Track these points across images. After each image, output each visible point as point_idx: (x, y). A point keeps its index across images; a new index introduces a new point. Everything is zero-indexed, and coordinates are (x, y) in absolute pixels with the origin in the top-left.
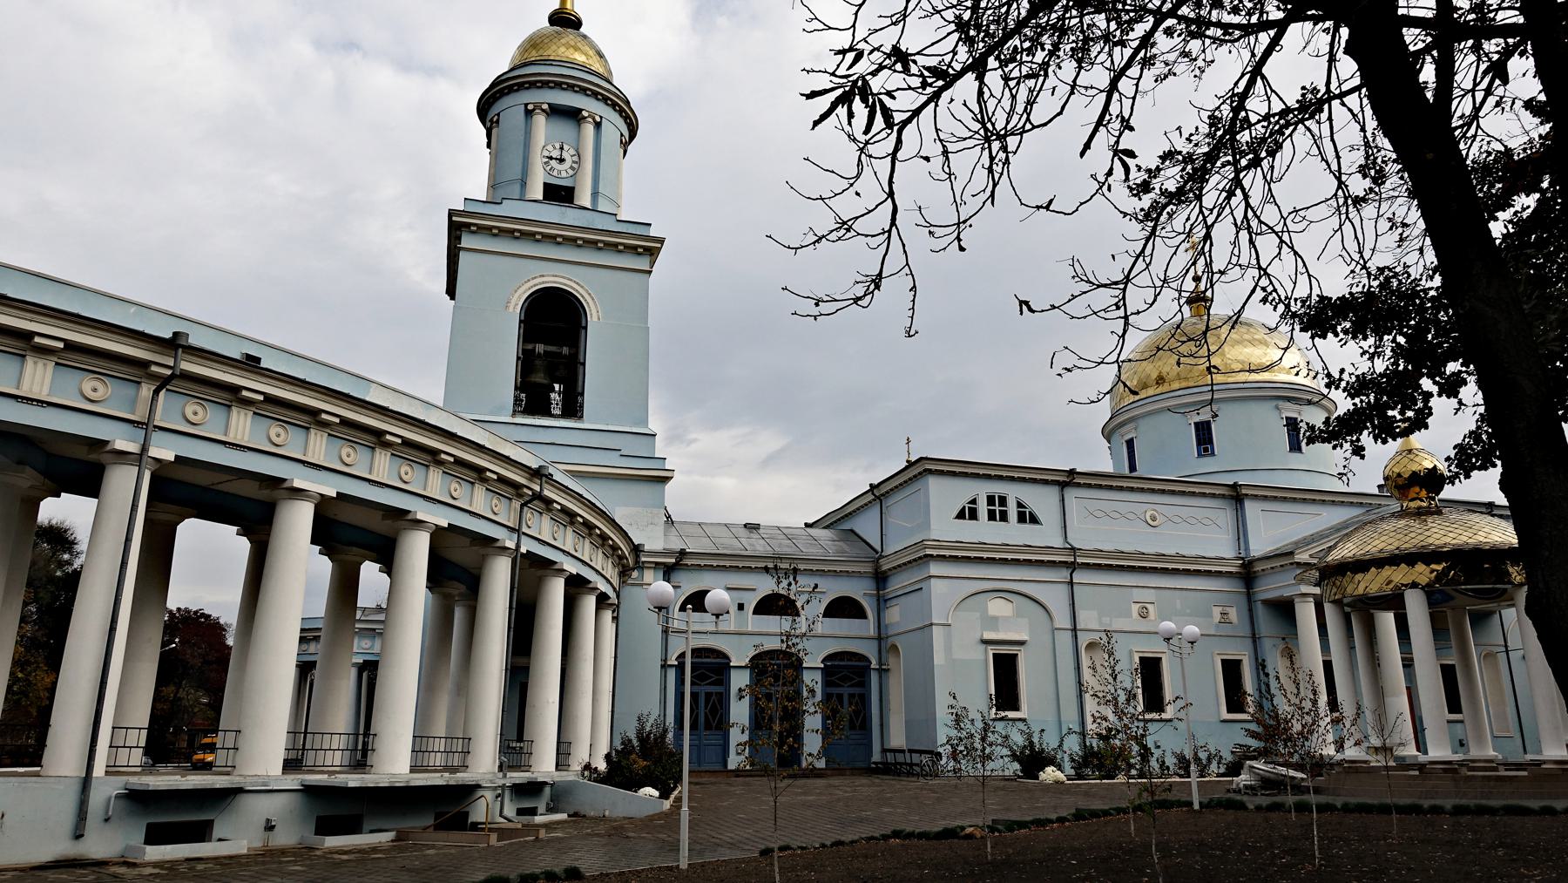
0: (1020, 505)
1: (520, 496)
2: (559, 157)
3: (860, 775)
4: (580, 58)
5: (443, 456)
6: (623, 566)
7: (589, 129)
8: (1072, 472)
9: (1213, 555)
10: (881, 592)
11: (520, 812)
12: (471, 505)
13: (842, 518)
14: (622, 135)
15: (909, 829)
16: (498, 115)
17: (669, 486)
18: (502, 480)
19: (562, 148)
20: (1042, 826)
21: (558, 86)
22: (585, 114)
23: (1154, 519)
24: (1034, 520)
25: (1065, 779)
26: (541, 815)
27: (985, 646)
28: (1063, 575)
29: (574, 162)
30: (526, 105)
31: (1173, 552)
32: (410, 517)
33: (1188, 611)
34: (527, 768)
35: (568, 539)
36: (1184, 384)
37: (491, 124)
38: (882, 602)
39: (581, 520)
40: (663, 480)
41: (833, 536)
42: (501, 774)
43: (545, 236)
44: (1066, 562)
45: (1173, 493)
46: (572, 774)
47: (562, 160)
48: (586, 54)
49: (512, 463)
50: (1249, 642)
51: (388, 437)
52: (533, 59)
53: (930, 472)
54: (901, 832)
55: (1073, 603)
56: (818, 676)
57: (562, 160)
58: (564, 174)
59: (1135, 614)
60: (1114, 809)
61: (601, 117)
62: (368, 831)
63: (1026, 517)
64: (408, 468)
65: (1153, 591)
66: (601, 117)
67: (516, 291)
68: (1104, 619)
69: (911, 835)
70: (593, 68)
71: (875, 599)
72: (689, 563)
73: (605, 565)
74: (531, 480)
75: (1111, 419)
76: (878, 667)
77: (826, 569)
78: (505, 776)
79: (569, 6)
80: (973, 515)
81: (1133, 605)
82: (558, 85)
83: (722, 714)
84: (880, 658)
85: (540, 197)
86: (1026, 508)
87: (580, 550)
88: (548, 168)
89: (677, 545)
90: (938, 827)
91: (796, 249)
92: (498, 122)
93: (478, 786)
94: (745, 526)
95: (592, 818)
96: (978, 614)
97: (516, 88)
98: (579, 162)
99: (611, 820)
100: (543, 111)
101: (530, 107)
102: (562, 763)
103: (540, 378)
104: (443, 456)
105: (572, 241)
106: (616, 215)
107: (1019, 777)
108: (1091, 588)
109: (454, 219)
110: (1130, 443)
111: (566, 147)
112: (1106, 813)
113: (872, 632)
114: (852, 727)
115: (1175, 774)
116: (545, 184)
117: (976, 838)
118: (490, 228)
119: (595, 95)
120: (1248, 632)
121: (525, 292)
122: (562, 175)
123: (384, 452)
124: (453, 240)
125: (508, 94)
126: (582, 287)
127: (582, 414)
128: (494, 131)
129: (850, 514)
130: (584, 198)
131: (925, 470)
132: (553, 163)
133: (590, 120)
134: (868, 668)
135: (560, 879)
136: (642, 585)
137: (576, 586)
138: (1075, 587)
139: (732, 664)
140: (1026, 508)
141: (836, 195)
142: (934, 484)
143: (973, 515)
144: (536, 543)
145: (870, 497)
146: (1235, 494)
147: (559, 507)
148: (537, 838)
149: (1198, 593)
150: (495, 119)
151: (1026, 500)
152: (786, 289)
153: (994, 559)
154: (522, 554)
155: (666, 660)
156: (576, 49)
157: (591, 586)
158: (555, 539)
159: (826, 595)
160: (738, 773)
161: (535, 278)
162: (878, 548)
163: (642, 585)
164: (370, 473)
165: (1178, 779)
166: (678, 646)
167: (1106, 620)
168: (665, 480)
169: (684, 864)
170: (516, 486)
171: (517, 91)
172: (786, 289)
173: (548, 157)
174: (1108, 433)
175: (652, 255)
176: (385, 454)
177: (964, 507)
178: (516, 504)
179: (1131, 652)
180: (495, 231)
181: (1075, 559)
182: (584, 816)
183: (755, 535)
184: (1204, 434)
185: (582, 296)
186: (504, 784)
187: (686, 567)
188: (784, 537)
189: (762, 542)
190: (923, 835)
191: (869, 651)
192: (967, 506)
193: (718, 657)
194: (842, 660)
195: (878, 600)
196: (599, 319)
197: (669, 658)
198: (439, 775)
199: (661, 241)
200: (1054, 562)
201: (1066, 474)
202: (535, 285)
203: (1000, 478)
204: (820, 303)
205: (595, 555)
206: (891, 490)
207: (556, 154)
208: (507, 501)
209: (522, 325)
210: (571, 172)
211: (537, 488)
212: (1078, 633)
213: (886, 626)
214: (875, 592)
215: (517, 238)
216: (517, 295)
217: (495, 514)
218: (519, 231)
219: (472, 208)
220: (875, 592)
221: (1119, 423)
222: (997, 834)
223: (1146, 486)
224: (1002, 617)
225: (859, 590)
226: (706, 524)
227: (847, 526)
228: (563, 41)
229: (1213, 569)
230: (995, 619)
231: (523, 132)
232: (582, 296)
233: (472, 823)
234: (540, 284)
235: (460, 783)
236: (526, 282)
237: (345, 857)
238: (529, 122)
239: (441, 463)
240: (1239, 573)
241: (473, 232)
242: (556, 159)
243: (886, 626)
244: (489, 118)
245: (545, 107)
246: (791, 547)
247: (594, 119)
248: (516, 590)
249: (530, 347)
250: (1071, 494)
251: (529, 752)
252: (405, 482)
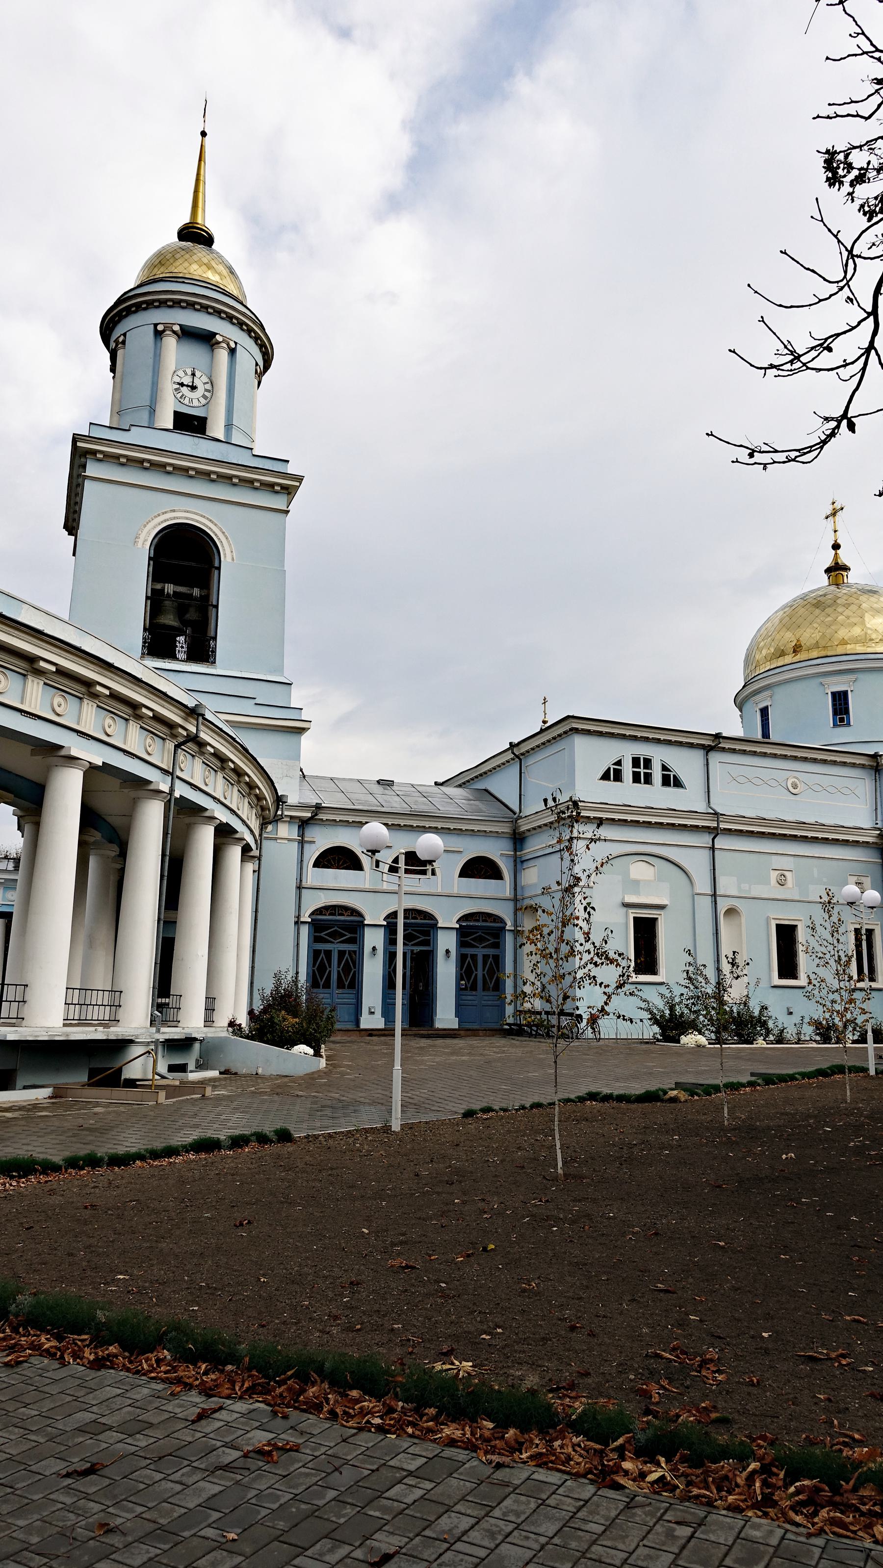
0: (664, 768)
1: (174, 736)
2: (190, 384)
3: (485, 1035)
4: (213, 277)
5: (99, 688)
6: (264, 818)
7: (222, 354)
8: (718, 736)
9: (851, 825)
10: (518, 853)
11: (172, 1068)
12: (125, 744)
13: (476, 777)
14: (257, 364)
15: (606, 1091)
16: (125, 335)
17: (305, 738)
18: (158, 718)
19: (193, 375)
20: (736, 1090)
21: (191, 306)
22: (218, 337)
23: (795, 786)
24: (678, 784)
25: (706, 1043)
26: (191, 1072)
27: (625, 909)
28: (705, 840)
29: (206, 390)
30: (156, 325)
31: (812, 821)
32: (63, 752)
33: (825, 880)
34: (176, 1023)
35: (218, 785)
36: (823, 653)
37: (117, 345)
38: (519, 863)
39: (232, 766)
40: (300, 731)
41: (468, 795)
42: (154, 1029)
43: (176, 468)
44: (708, 827)
45: (815, 761)
46: (220, 1030)
47: (193, 388)
48: (220, 274)
49: (169, 700)
51: (42, 664)
52: (164, 275)
53: (576, 731)
54: (598, 1094)
55: (714, 869)
56: (453, 936)
57: (193, 388)
58: (196, 403)
59: (773, 881)
60: (799, 1074)
61: (236, 343)
62: (21, 1088)
63: (670, 780)
64: (61, 700)
65: (792, 858)
66: (236, 343)
67: (145, 526)
68: (742, 885)
69: (607, 1098)
70: (226, 289)
71: (512, 859)
72: (325, 818)
74: (186, 720)
75: (744, 687)
76: (513, 928)
77: (464, 828)
78: (158, 1031)
79: (200, 221)
80: (618, 777)
81: (772, 871)
82: (191, 305)
83: (355, 972)
84: (515, 920)
85: (171, 427)
86: (671, 771)
87: (229, 798)
88: (179, 396)
89: (313, 800)
90: (637, 1088)
91: (765, 369)
92: (124, 342)
93: (131, 1042)
94: (378, 782)
95: (245, 1076)
96: (620, 877)
97: (133, 309)
98: (211, 391)
99: (270, 1078)
100: (174, 332)
101: (160, 328)
102: (209, 1021)
103: (169, 620)
104: (99, 688)
106: (252, 449)
107: (658, 1040)
108: (732, 853)
109: (79, 444)
110: (764, 712)
111: (198, 374)
112: (792, 1077)
113: (508, 893)
114: (340, 985)
115: (811, 1040)
116: (176, 413)
117: (680, 1102)
118: (117, 457)
119: (230, 318)
121: (159, 524)
122: (193, 404)
123: (36, 681)
124: (76, 467)
125: (135, 312)
126: (216, 525)
127: (215, 659)
128: (120, 353)
129: (485, 773)
130: (217, 429)
131: (571, 729)
132: (184, 390)
133: (224, 345)
134: (503, 929)
135: (272, 1141)
136: (276, 839)
137: (224, 833)
138: (716, 852)
139: (366, 922)
140: (671, 771)
141: (820, 301)
142: (579, 742)
143: (618, 777)
144: (188, 787)
145: (509, 756)
146: (875, 764)
147: (212, 751)
148: (203, 1096)
149: (834, 863)
150: (121, 339)
151: (671, 764)
152: (712, 435)
153: (638, 822)
154: (176, 799)
155: (298, 917)
156: (209, 267)
157: (237, 836)
158: (206, 785)
159: (463, 854)
160: (371, 1032)
161: (166, 512)
162: (517, 810)
163: (276, 839)
164: (22, 703)
165: (815, 1045)
166: (313, 902)
167: (745, 886)
168: (301, 731)
169: (396, 1126)
170: (171, 726)
171: (145, 309)
172: (712, 435)
173: (179, 384)
174: (740, 702)
175: (289, 494)
176: (38, 683)
177: (609, 768)
178: (170, 745)
179: (768, 919)
180: (123, 460)
181: (718, 824)
182: (236, 1074)
183: (389, 792)
184: (840, 704)
185: (216, 535)
186: (158, 1040)
187: (320, 822)
188: (418, 794)
189: (397, 799)
190: (621, 1098)
191: (505, 912)
192: (612, 767)
193: (352, 915)
194: (478, 921)
195: (515, 861)
196: (233, 559)
197: (302, 915)
198: (93, 1029)
199: (300, 479)
200: (697, 826)
201: (712, 738)
202: (165, 521)
203: (646, 739)
204: (755, 454)
205: (242, 804)
206: (533, 749)
207: (187, 380)
208: (161, 741)
209: (152, 563)
210: (203, 401)
211: (193, 729)
212: (718, 898)
213: (522, 888)
214: (512, 853)
215: (146, 469)
216: (146, 530)
217: (149, 754)
218: (149, 461)
219: (97, 433)
220: (512, 853)
221: (754, 691)
222: (696, 1097)
223: (789, 753)
224: (642, 880)
226: (338, 779)
227: (481, 785)
228: (195, 258)
229: (851, 838)
230: (637, 882)
231: (151, 355)
232: (216, 535)
233: (125, 1079)
234: (171, 519)
235: (120, 1038)
236: (155, 517)
237: (9, 1115)
238: (159, 345)
239: (95, 696)
240: (876, 843)
241: (100, 460)
242: (188, 386)
243: (522, 888)
244: (113, 338)
245: (176, 328)
246: (428, 805)
247: (228, 345)
248: (169, 836)
249: (158, 586)
250: (715, 758)
251: (178, 1007)
252: (58, 715)
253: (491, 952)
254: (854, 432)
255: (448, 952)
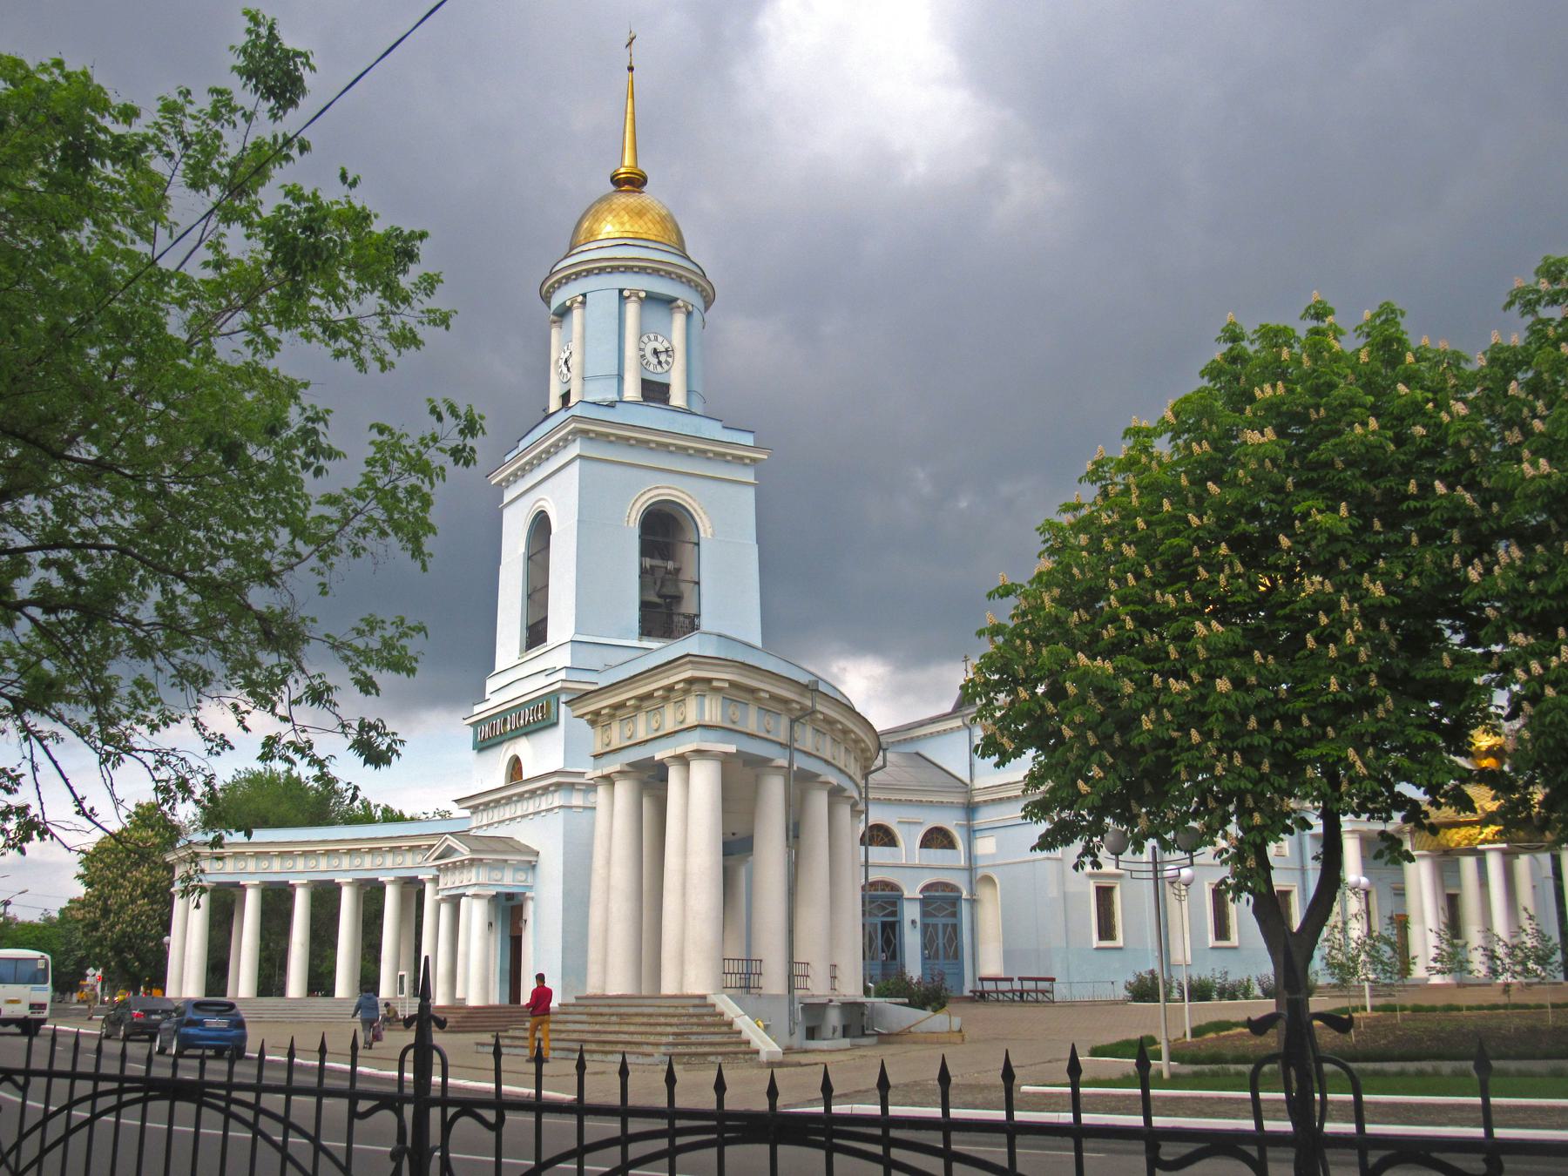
38: (971, 832)
50: (1298, 873)
73: (836, 754)
101: (626, 293)
105: (683, 450)
113: (963, 862)
114: (946, 957)
120: (1297, 866)
162: (967, 780)
170: (785, 702)
178: (784, 722)
191: (960, 881)
218: (635, 439)
225: (951, 821)
253: (950, 921)
254: (343, 169)
255: (913, 922)
